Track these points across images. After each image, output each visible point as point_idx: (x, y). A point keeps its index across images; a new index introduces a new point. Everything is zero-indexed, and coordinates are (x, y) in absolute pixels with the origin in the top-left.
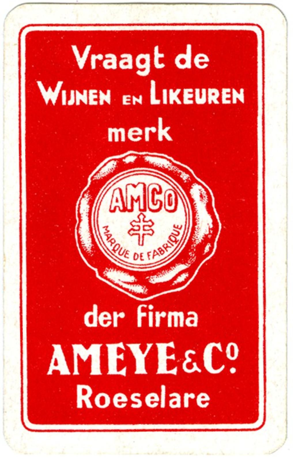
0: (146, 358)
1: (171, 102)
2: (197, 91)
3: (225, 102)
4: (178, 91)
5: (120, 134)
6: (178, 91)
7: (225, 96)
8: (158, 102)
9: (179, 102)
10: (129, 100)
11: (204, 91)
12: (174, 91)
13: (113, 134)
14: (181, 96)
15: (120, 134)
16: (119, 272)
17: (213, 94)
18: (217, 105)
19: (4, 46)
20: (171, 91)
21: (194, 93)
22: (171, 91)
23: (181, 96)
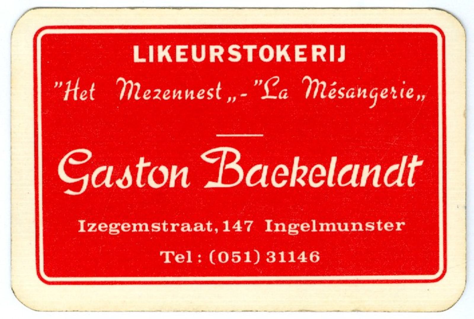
1: (160, 60)
2: (194, 48)
8: (143, 60)
22: (160, 48)
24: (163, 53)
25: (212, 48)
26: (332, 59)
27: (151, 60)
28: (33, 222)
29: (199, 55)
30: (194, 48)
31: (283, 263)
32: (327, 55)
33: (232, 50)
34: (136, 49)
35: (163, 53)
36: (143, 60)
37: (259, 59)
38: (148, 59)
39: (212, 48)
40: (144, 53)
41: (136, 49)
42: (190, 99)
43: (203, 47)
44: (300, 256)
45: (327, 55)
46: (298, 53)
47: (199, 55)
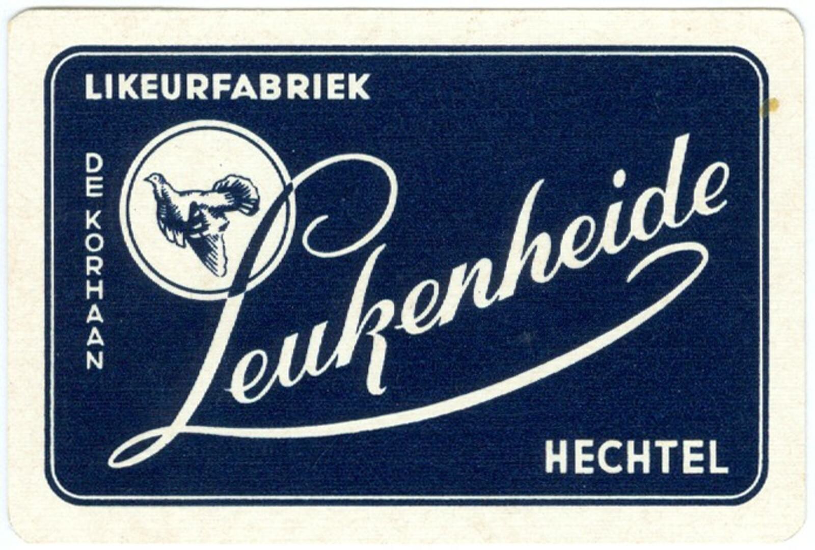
0: (692, 202)
1: (122, 96)
2: (165, 78)
3: (332, 95)
4: (133, 77)
5: (92, 183)
6: (133, 77)
7: (332, 87)
8: (98, 96)
9: (134, 96)
10: (155, 87)
11: (177, 78)
12: (358, 78)
13: (92, 191)
14: (137, 86)
15: (92, 183)
16: (534, 263)
17: (298, 83)
18: (203, 101)
19: (806, 401)
20: (122, 77)
21: (159, 82)
22: (122, 77)
23: (137, 86)
24: (125, 86)
25: (191, 78)
26: (317, 95)
27: (109, 95)
28: (427, 15)
29: (171, 89)
30: (165, 78)
31: (105, 287)
32: (310, 90)
33: (573, 257)
34: (89, 78)
35: (125, 86)
36: (98, 96)
37: (596, 223)
38: (104, 94)
39: (191, 78)
40: (99, 87)
41: (89, 78)
42: (230, 96)
43: (177, 78)
44: (98, 335)
45: (310, 90)
46: (145, 87)
47: (171, 89)
